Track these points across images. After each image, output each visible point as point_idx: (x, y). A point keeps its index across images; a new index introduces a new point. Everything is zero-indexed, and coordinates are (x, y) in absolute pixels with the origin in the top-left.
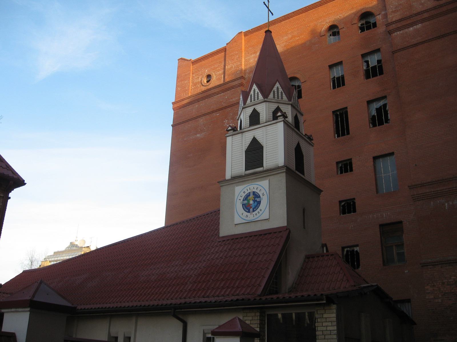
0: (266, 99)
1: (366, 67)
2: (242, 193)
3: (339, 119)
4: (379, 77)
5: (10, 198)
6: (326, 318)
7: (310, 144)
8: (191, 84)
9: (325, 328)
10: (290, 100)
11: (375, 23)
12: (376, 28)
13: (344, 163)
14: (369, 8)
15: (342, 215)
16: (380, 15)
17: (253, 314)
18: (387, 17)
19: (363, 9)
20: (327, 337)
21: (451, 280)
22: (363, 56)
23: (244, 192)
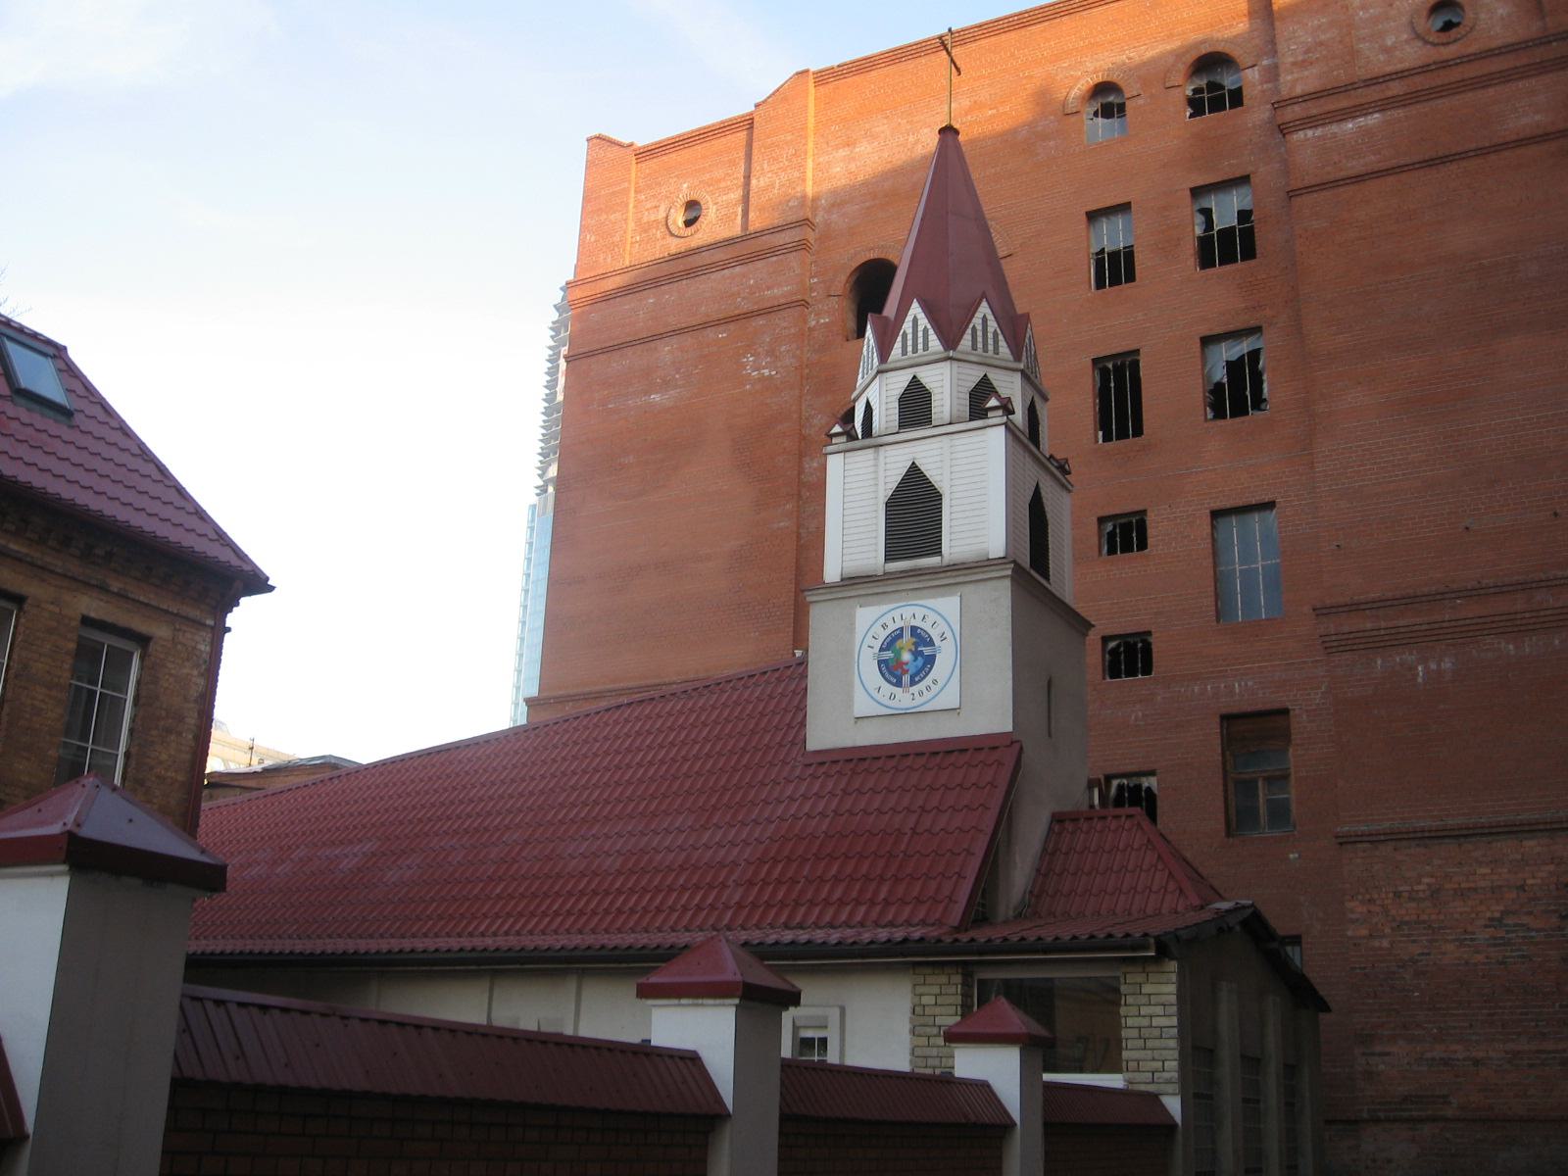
0: (951, 353)
1: (1204, 227)
2: (877, 628)
3: (1112, 385)
4: (1240, 265)
5: (229, 630)
6: (1150, 995)
7: (1063, 486)
8: (631, 225)
9: (1145, 1022)
10: (1018, 359)
11: (1240, 89)
12: (1240, 108)
13: (1123, 521)
14: (1222, 41)
15: (1108, 680)
16: (1256, 68)
17: (943, 979)
18: (1278, 75)
19: (1203, 42)
20: (1150, 1044)
21: (1421, 887)
22: (1197, 192)
23: (884, 626)
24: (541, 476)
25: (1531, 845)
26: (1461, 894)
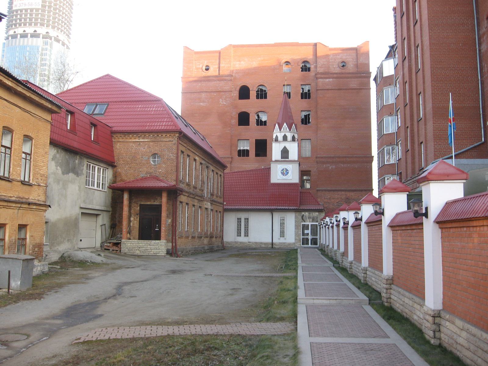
11: (310, 68)
24: (6, 33)
25: (343, 193)
26: (333, 199)
